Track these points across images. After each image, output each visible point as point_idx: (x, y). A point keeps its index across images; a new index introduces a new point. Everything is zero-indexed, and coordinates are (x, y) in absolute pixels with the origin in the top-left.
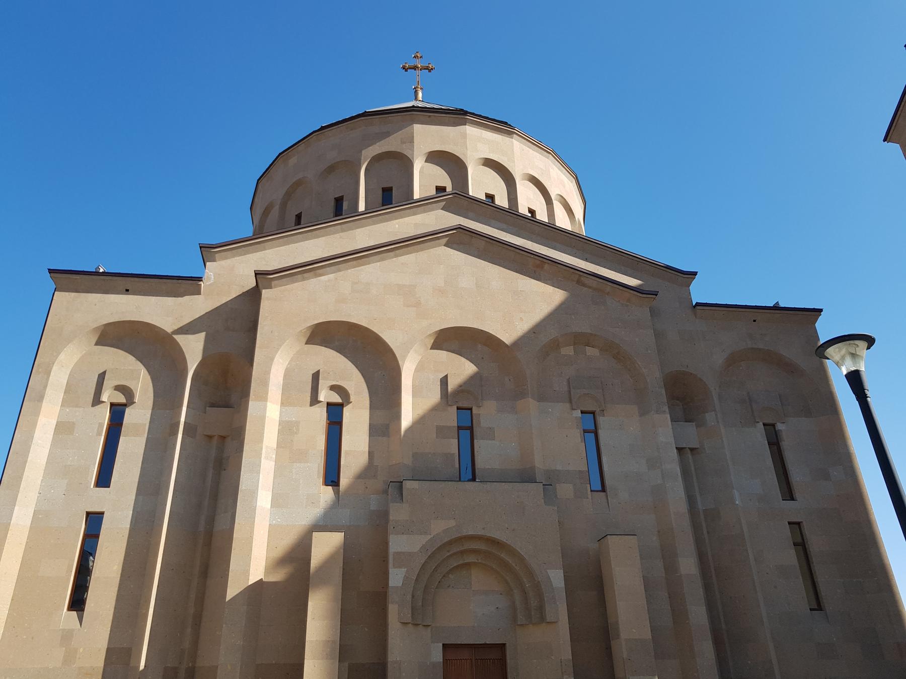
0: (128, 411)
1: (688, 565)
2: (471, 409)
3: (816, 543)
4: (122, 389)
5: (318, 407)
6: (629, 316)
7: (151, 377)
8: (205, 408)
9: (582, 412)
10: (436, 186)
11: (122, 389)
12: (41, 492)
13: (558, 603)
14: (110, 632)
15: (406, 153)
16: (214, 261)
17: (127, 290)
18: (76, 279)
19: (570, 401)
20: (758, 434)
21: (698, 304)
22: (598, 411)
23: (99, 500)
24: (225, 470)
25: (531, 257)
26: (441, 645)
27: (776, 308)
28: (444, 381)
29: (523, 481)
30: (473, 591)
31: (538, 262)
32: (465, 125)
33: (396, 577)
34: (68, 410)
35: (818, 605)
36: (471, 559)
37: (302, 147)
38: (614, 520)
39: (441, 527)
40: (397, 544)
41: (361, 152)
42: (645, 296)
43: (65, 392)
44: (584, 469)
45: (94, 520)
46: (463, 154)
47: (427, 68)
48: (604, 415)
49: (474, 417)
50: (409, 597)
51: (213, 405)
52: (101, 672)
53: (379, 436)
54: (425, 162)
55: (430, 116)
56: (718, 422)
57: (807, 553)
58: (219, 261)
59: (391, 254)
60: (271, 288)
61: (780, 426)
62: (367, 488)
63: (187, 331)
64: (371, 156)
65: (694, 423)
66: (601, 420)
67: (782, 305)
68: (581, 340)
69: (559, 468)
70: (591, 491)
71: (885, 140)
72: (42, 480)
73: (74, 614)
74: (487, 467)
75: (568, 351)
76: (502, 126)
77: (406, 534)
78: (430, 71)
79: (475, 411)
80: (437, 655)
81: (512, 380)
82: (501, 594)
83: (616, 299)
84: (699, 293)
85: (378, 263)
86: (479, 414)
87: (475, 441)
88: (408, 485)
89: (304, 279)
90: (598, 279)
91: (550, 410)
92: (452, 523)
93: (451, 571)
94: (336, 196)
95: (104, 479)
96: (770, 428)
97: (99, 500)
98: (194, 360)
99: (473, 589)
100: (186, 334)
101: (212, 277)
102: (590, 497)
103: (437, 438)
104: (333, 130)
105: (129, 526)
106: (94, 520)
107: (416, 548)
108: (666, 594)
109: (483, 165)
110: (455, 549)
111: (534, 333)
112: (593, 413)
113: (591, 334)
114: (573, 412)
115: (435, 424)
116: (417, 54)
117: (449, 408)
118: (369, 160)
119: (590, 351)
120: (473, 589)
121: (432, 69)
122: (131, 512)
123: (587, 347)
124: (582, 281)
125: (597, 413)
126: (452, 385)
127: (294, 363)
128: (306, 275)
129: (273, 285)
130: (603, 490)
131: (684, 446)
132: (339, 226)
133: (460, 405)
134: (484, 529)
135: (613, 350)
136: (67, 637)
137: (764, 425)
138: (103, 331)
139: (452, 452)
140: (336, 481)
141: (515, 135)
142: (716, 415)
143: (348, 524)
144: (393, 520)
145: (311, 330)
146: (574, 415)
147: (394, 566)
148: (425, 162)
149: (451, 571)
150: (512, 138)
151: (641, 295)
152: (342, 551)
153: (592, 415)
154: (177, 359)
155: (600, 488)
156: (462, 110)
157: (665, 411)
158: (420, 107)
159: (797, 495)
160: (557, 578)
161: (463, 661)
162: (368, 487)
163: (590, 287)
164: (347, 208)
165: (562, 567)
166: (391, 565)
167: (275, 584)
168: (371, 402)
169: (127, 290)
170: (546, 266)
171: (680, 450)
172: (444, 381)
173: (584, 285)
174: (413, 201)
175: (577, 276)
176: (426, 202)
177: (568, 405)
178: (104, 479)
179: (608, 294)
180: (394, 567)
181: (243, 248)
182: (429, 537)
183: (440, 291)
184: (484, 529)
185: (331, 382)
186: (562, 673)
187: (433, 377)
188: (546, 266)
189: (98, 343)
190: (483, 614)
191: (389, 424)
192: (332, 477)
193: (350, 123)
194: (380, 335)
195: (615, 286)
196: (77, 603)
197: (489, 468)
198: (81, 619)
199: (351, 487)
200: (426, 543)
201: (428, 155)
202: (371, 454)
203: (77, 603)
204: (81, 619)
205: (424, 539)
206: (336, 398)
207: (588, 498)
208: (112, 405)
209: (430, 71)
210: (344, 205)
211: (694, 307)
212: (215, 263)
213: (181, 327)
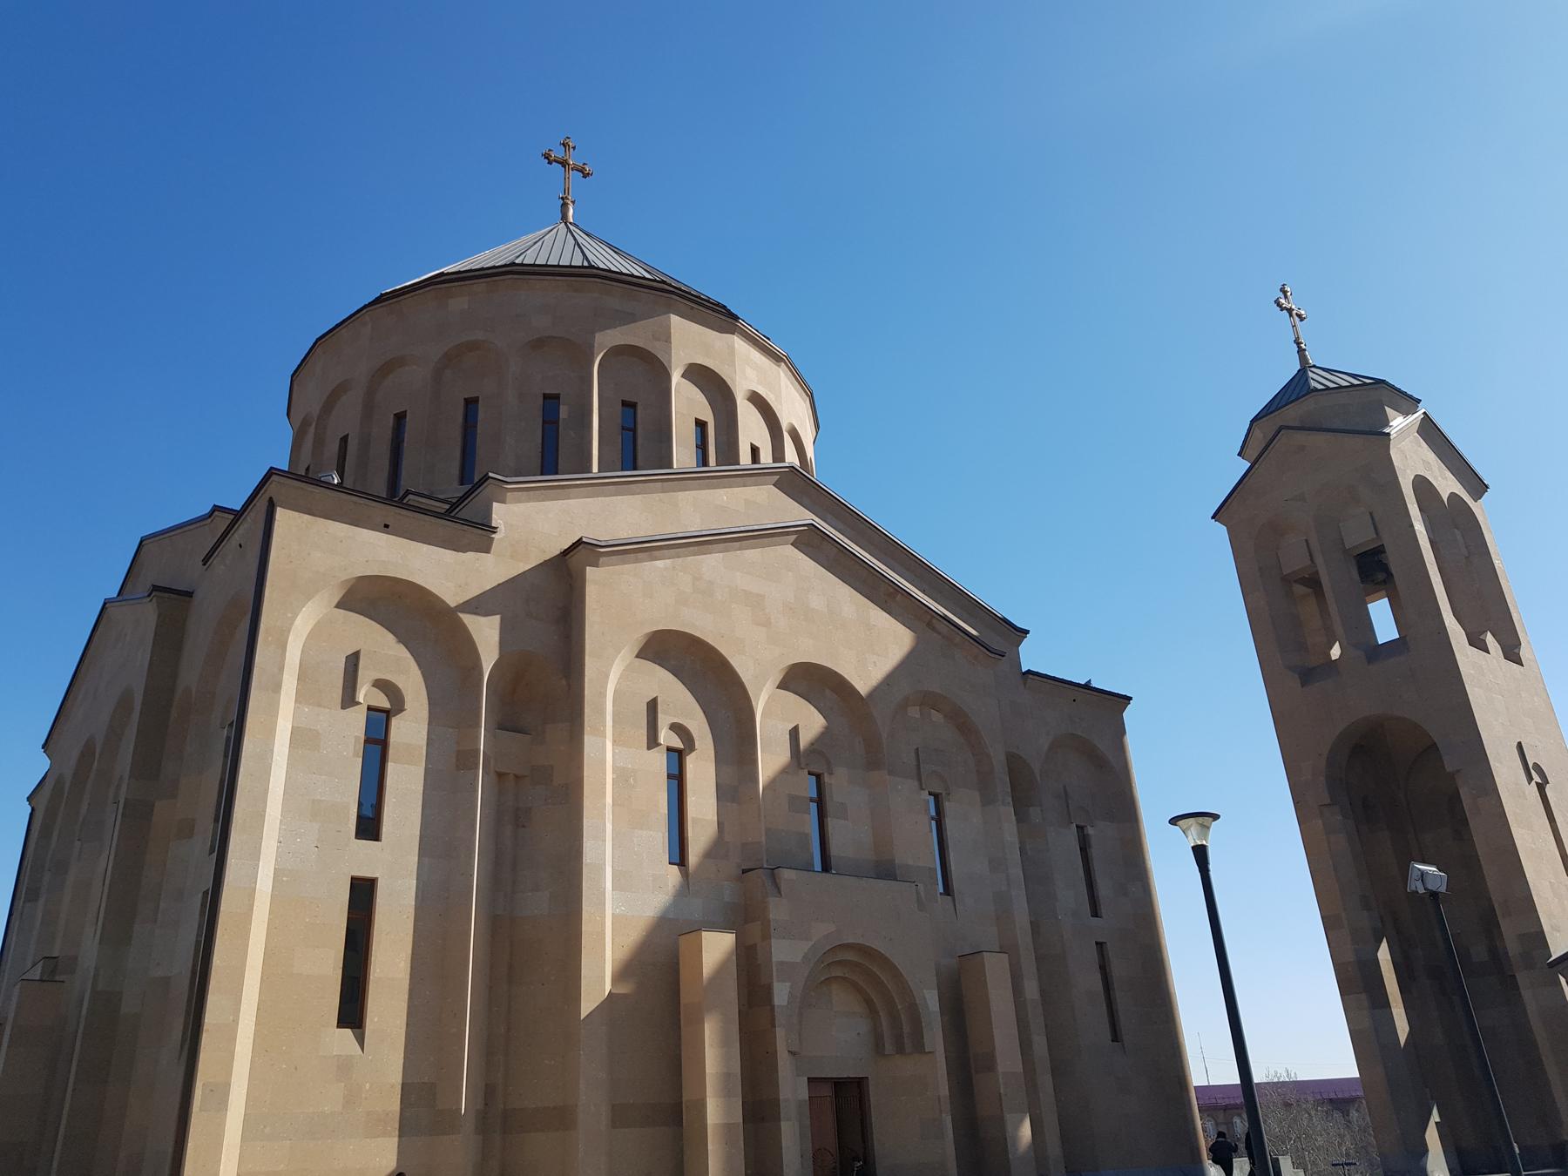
0: (394, 722)
3: (1118, 969)
4: (382, 685)
5: (658, 752)
7: (422, 673)
11: (382, 685)
12: (281, 839)
14: (404, 1058)
15: (655, 348)
16: (503, 502)
17: (386, 526)
18: (312, 492)
19: (920, 780)
20: (1072, 836)
21: (1029, 672)
23: (366, 859)
24: (524, 826)
26: (806, 1079)
27: (1087, 686)
28: (794, 733)
29: (879, 877)
31: (892, 590)
32: (734, 334)
34: (307, 710)
35: (1116, 1037)
37: (480, 286)
41: (593, 333)
42: (993, 655)
43: (298, 679)
45: (363, 893)
46: (732, 380)
47: (582, 170)
52: (398, 1118)
54: (682, 376)
55: (692, 308)
57: (1107, 978)
58: (511, 503)
59: (737, 544)
60: (597, 567)
61: (1090, 831)
63: (477, 608)
64: (610, 346)
67: (1094, 684)
68: (929, 701)
69: (910, 862)
71: (1213, 518)
72: (281, 821)
73: (348, 1032)
76: (721, 317)
78: (585, 177)
84: (1032, 657)
85: (721, 555)
88: (787, 875)
89: (637, 561)
90: (950, 626)
94: (547, 392)
95: (369, 827)
96: (1080, 828)
97: (366, 859)
98: (489, 657)
100: (475, 614)
104: (545, 282)
105: (414, 903)
106: (363, 893)
109: (748, 400)
111: (888, 685)
116: (568, 140)
117: (800, 771)
118: (605, 351)
121: (588, 174)
122: (415, 881)
126: (805, 739)
128: (640, 555)
129: (600, 562)
132: (660, 483)
133: (811, 770)
135: (961, 722)
136: (344, 1067)
137: (1077, 826)
138: (352, 586)
141: (783, 364)
145: (647, 639)
148: (682, 376)
150: (779, 366)
151: (988, 653)
152: (734, 958)
154: (467, 648)
156: (724, 307)
158: (692, 295)
159: (1104, 910)
163: (939, 633)
164: (566, 417)
167: (624, 995)
168: (716, 752)
169: (386, 526)
170: (899, 597)
172: (794, 733)
173: (934, 629)
174: (738, 467)
175: (929, 617)
176: (756, 474)
177: (916, 783)
178: (369, 827)
180: (778, 981)
181: (543, 491)
186: (941, 1111)
189: (340, 605)
192: (679, 856)
193: (576, 281)
194: (729, 659)
196: (352, 1013)
198: (361, 1041)
199: (700, 865)
201: (688, 368)
202: (720, 824)
203: (352, 1013)
204: (361, 1041)
205: (805, 946)
206: (677, 743)
208: (370, 708)
209: (585, 177)
210: (561, 411)
211: (1024, 673)
212: (503, 505)
213: (467, 601)
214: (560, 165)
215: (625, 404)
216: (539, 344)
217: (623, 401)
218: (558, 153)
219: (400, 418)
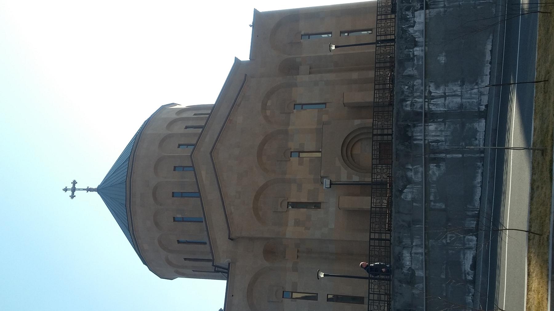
1: (355, 75)
2: (291, 152)
8: (286, 259)
9: (294, 109)
19: (290, 113)
22: (294, 103)
24: (311, 250)
39: (338, 162)
40: (344, 178)
48: (296, 101)
49: (295, 151)
51: (285, 257)
56: (300, 57)
65: (300, 66)
66: (298, 102)
70: (326, 108)
75: (268, 113)
79: (292, 151)
87: (305, 151)
88: (322, 174)
93: (354, 161)
101: (227, 260)
102: (328, 109)
110: (346, 158)
112: (295, 105)
114: (294, 112)
119: (269, 103)
123: (267, 105)
125: (284, 290)
127: (444, 134)
130: (325, 104)
133: (290, 156)
140: (206, 240)
149: (354, 161)
153: (292, 153)
155: (325, 105)
160: (357, 122)
170: (231, 119)
171: (310, 73)
214: (75, 192)
215: (174, 170)
216: (157, 224)
217: (174, 171)
218: (70, 193)
219: (185, 259)
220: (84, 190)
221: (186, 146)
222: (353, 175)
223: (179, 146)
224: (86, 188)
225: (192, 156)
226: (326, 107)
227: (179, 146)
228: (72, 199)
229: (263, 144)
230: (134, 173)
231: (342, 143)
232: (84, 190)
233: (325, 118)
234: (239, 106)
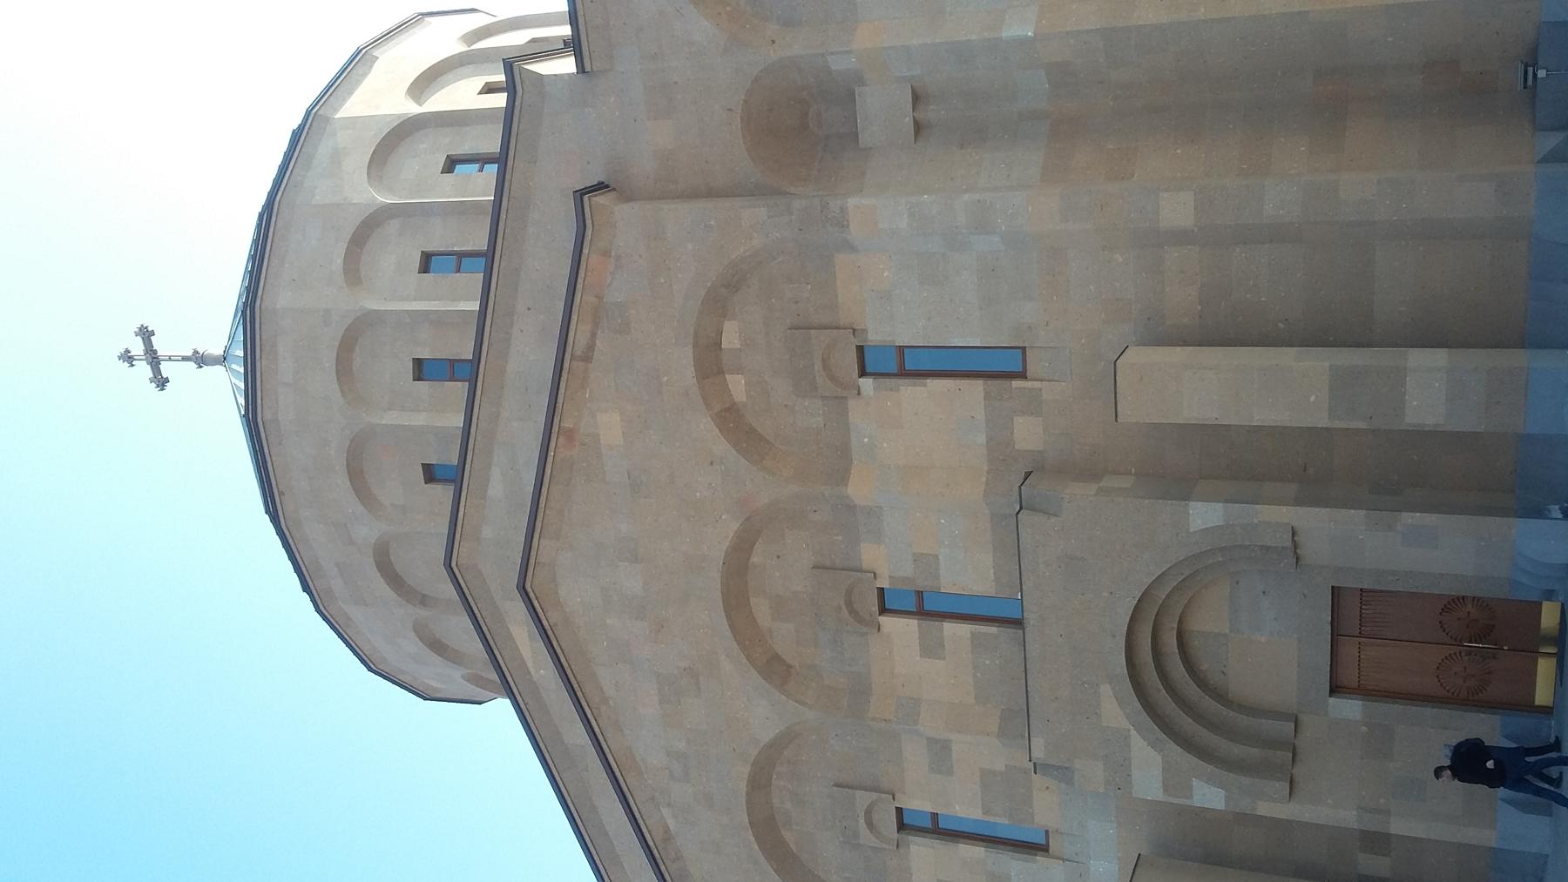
6: (640, 256)
10: (414, 380)
13: (1255, 521)
25: (554, 456)
26: (1332, 700)
30: (1230, 632)
33: (1209, 795)
36: (1191, 690)
38: (1083, 341)
42: (589, 222)
44: (981, 388)
48: (864, 331)
50: (1246, 781)
53: (951, 756)
62: (1047, 788)
69: (982, 439)
74: (992, 575)
77: (1130, 771)
80: (1349, 709)
81: (815, 508)
82: (1237, 583)
83: (608, 281)
86: (890, 577)
91: (866, 440)
92: (1106, 689)
99: (1227, 631)
102: (1037, 384)
103: (944, 659)
107: (1157, 758)
108: (1238, 250)
113: (695, 345)
115: (918, 658)
117: (884, 629)
119: (731, 337)
120: (1227, 631)
124: (583, 352)
131: (909, 121)
133: (875, 609)
134: (1114, 636)
139: (969, 635)
142: (832, 54)
143: (1115, 825)
144: (1106, 788)
146: (872, 393)
147: (1187, 798)
157: (841, 208)
161: (1363, 607)
162: (1047, 785)
163: (594, 335)
165: (1183, 503)
166: (1188, 802)
170: (567, 424)
173: (591, 347)
175: (575, 364)
179: (600, 297)
180: (1191, 797)
182: (1133, 732)
183: (659, 631)
184: (1114, 636)
185: (860, 824)
187: (828, 652)
188: (567, 424)
190: (1275, 619)
191: (928, 739)
195: (579, 286)
197: (995, 573)
200: (1145, 740)
205: (1139, 745)
207: (1040, 390)
218: (143, 369)
220: (185, 359)
221: (477, 166)
222: (1195, 782)
223: (451, 164)
224: (189, 354)
225: (454, 564)
226: (1018, 616)
227: (451, 164)
228: (162, 389)
229: (741, 548)
230: (281, 494)
231: (1126, 628)
232: (185, 359)
233: (1028, 434)
234: (587, 357)
